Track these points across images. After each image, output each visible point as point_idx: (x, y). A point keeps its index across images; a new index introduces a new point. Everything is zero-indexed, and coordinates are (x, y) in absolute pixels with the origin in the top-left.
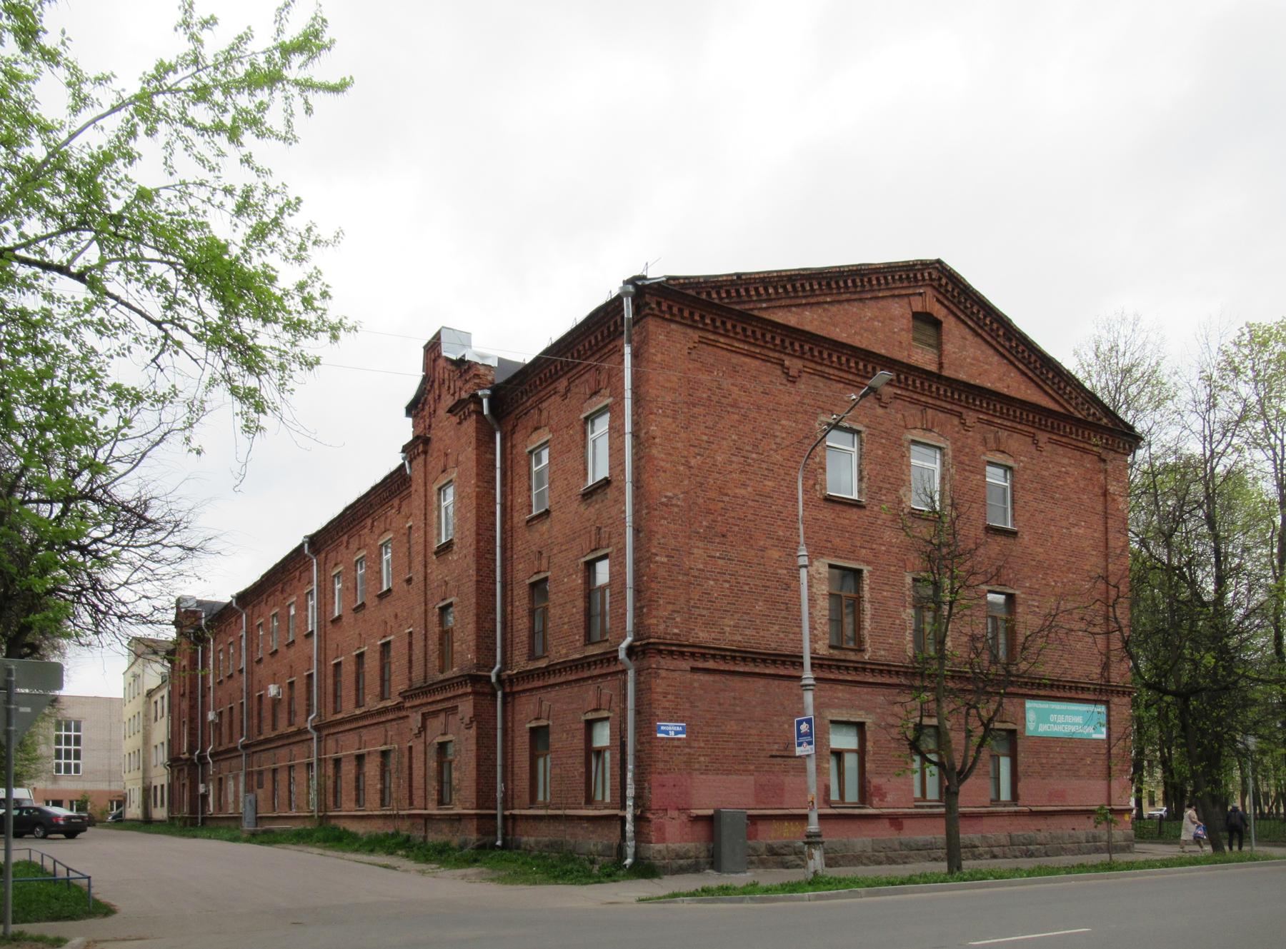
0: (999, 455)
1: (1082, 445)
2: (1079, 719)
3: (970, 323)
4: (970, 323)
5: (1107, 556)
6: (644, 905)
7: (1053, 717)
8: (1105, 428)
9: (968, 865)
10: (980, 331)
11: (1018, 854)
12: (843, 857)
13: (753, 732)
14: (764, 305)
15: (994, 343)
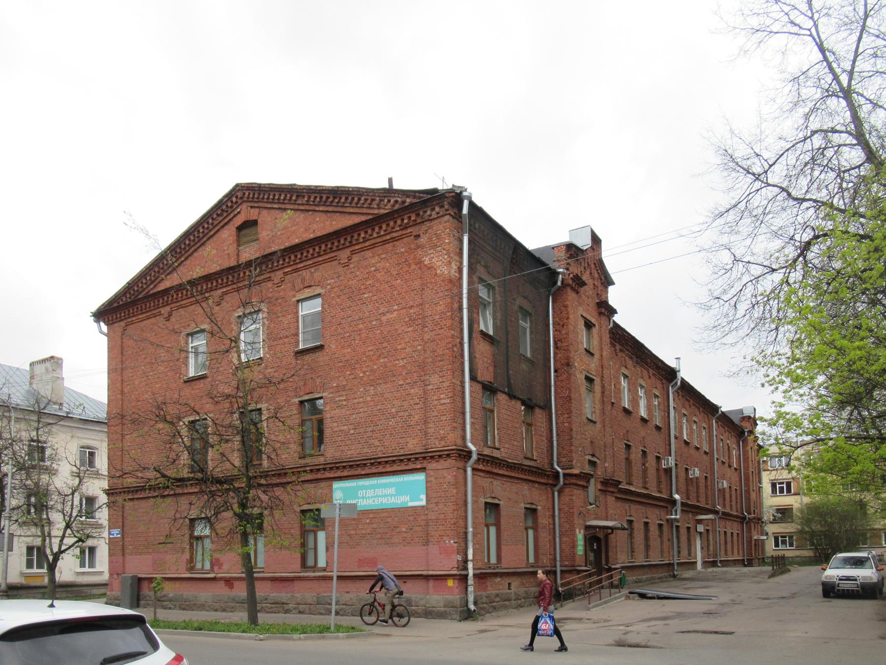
0: (307, 290)
1: (388, 237)
2: (392, 491)
3: (275, 206)
4: (275, 206)
6: (607, 647)
7: (360, 493)
8: (412, 205)
9: (262, 617)
11: (322, 611)
12: (194, 604)
13: (151, 530)
14: (152, 286)
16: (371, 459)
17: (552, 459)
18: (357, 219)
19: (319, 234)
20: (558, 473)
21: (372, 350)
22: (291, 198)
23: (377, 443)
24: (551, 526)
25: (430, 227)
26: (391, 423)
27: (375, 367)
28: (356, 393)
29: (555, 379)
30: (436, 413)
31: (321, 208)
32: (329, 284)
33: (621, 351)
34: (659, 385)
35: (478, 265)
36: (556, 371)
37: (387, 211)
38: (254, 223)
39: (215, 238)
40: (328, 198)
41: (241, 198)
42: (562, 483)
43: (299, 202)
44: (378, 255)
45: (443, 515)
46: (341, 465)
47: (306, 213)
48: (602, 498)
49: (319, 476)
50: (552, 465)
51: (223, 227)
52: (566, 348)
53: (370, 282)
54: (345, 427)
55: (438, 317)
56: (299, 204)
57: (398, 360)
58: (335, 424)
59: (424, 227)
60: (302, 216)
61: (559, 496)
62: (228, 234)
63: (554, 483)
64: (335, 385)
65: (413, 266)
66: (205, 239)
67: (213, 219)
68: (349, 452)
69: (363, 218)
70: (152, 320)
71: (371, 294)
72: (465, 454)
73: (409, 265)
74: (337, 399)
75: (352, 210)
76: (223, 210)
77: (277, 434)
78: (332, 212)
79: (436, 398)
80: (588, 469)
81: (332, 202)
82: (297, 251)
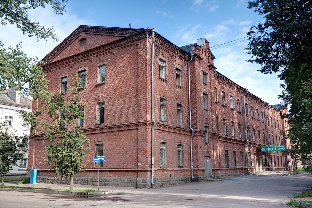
0: (101, 63)
1: (128, 45)
5: (138, 76)
10: (95, 33)
15: (99, 34)
16: (119, 125)
17: (190, 125)
18: (118, 38)
19: (106, 43)
20: (192, 131)
21: (121, 85)
22: (97, 31)
23: (122, 119)
24: (189, 152)
25: (142, 42)
26: (127, 112)
27: (122, 91)
28: (115, 100)
29: (191, 95)
30: (141, 108)
31: (107, 34)
32: (108, 61)
33: (221, 83)
34: (239, 95)
35: (159, 54)
36: (191, 91)
37: (128, 36)
38: (85, 39)
39: (72, 44)
40: (109, 31)
41: (81, 30)
42: (193, 135)
43: (100, 32)
44: (125, 51)
45: (143, 147)
46: (109, 127)
47: (102, 36)
48: (211, 140)
49: (101, 131)
50: (190, 127)
51: (75, 40)
52: (194, 83)
53: (122, 60)
54: (112, 113)
55: (143, 73)
56: (100, 33)
57: (130, 88)
58: (108, 112)
59: (139, 41)
60: (101, 37)
61: (192, 140)
62: (77, 42)
63: (190, 135)
64: (109, 97)
65: (136, 55)
66: (69, 44)
67: (72, 38)
68: (113, 122)
69: (120, 38)
70: (50, 73)
71: (122, 64)
72: (151, 123)
73: (134, 55)
74: (109, 102)
75: (117, 35)
76: (75, 34)
77: (89, 115)
78: (110, 36)
79: (141, 102)
80: (204, 129)
81: (110, 32)
82: (98, 49)
